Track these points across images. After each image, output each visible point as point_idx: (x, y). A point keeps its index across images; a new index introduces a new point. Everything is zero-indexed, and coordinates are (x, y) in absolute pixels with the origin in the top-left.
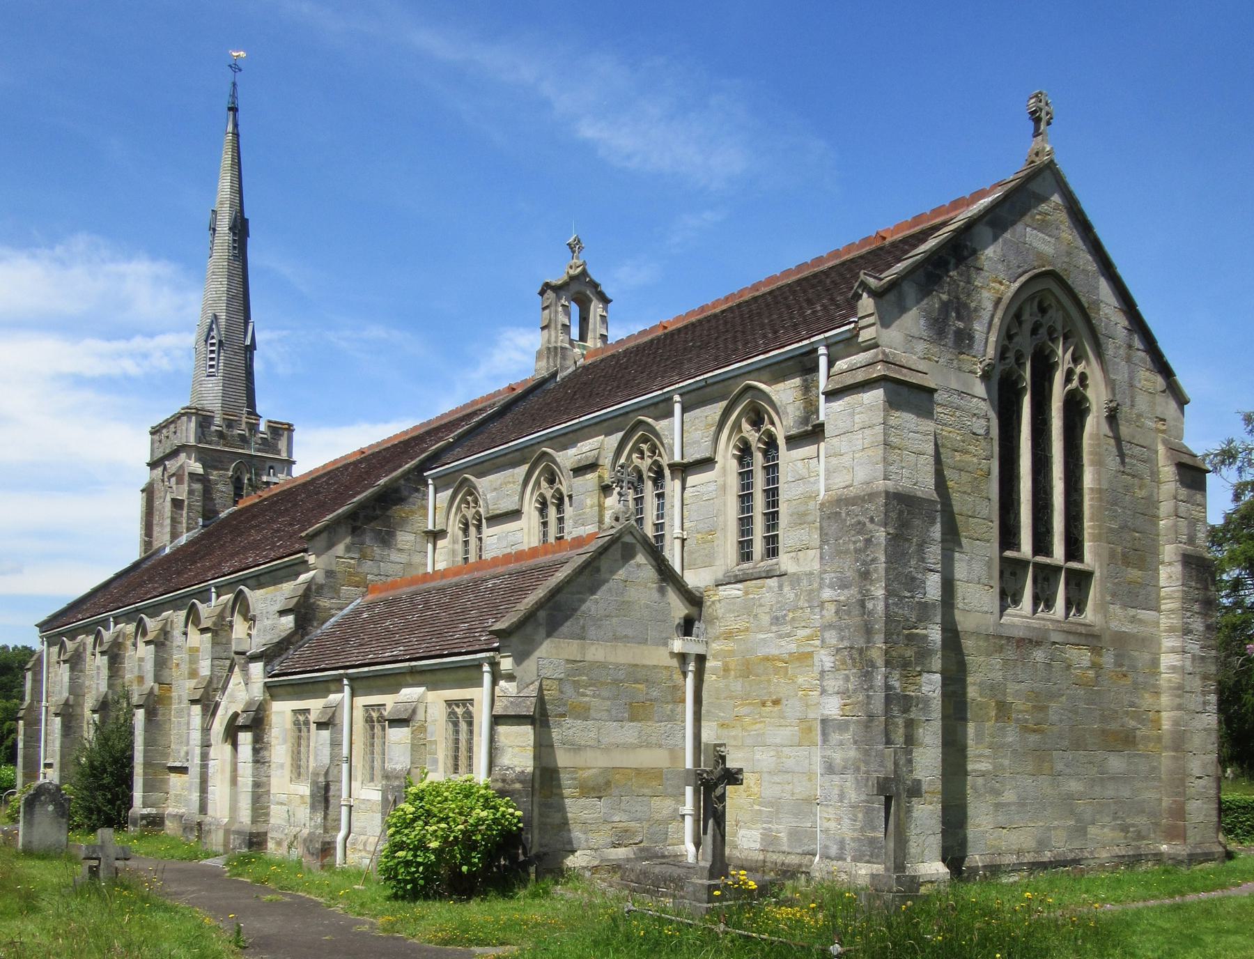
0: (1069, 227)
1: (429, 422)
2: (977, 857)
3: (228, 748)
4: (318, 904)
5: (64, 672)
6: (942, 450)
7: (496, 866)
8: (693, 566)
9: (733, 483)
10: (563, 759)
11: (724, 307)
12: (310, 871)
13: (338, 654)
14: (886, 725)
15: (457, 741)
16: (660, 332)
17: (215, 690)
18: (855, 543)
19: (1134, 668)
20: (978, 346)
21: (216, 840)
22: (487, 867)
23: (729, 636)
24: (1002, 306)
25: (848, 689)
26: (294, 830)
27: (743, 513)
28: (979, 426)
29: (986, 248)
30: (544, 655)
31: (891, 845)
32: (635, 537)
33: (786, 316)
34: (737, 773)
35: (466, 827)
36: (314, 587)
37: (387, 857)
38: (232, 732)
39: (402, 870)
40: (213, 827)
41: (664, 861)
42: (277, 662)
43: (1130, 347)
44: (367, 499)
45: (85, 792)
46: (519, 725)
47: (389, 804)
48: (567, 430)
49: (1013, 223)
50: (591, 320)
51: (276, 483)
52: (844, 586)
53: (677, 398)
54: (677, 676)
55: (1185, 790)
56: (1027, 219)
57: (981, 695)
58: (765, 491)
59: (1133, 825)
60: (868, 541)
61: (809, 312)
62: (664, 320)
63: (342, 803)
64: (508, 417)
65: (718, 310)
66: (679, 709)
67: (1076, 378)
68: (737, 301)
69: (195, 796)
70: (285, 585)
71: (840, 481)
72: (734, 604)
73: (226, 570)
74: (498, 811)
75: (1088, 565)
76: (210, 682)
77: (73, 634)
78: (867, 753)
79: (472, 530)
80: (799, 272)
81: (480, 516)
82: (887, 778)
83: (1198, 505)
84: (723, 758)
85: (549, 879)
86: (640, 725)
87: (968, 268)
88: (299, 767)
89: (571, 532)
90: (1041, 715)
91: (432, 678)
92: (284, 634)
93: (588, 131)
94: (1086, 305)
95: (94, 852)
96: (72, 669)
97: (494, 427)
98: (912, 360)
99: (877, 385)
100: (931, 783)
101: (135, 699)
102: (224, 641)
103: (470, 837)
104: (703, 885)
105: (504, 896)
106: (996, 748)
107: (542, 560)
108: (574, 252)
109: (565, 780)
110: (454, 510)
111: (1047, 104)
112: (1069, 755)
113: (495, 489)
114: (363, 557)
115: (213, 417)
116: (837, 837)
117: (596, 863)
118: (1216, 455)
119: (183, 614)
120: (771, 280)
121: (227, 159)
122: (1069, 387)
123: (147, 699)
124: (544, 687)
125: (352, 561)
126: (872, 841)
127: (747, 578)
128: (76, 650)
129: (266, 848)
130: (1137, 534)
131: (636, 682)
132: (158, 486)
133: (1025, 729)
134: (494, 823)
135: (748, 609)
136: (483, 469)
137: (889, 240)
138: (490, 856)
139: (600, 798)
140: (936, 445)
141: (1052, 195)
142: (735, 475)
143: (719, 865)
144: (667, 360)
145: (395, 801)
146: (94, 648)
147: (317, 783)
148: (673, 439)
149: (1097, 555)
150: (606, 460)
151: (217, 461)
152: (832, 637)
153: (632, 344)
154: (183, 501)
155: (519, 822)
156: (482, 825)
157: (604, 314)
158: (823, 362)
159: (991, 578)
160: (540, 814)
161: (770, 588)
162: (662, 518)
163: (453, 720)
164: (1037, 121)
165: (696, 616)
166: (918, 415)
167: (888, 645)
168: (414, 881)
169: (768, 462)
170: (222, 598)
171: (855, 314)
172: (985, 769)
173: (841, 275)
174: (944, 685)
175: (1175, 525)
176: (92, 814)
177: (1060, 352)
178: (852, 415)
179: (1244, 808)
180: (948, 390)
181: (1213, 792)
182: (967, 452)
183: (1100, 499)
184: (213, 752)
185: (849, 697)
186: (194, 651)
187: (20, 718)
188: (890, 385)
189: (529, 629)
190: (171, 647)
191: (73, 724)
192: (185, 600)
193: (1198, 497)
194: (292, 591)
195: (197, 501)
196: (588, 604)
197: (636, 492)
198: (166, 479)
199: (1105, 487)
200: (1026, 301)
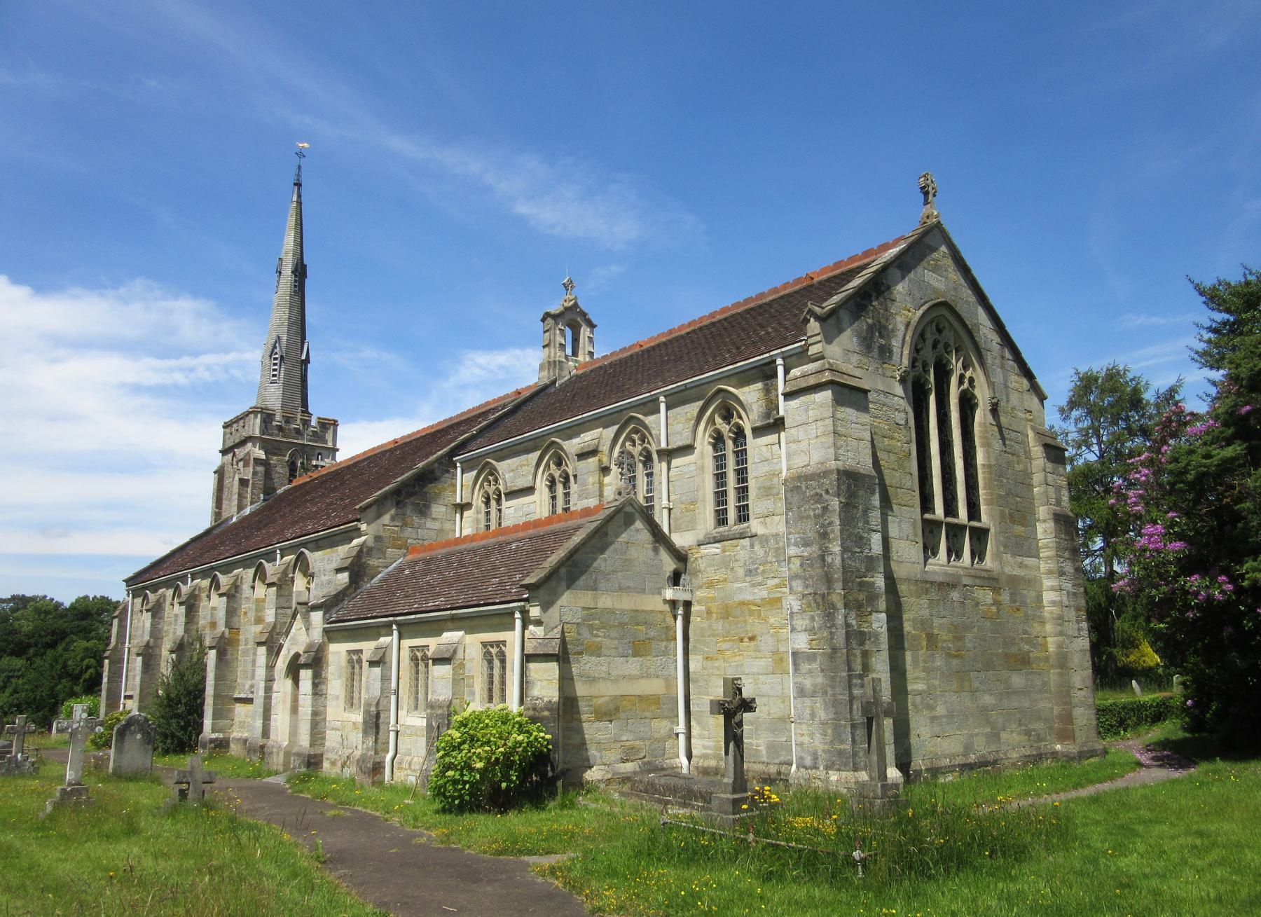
1: (451, 419)
3: (289, 682)
4: (376, 818)
5: (147, 619)
6: (874, 437)
8: (678, 530)
9: (709, 464)
10: (581, 690)
11: (688, 330)
12: (362, 787)
14: (848, 656)
15: (491, 676)
16: (637, 350)
18: (814, 510)
19: (1024, 604)
20: (896, 357)
21: (277, 761)
22: (523, 782)
23: (710, 585)
25: (814, 628)
26: (347, 752)
27: (718, 488)
30: (565, 604)
31: (875, 758)
34: (751, 702)
36: (365, 550)
37: (436, 776)
38: (294, 670)
39: (451, 788)
40: (275, 750)
42: (334, 610)
43: (1003, 357)
44: (409, 479)
45: (161, 720)
46: (546, 662)
47: (434, 731)
49: (915, 267)
50: (581, 341)
51: (322, 467)
52: (806, 544)
53: (662, 399)
54: (670, 619)
55: (1071, 701)
56: (924, 263)
58: (735, 470)
59: (1034, 730)
60: (825, 509)
64: (519, 415)
65: (683, 332)
66: (672, 645)
67: (966, 381)
68: (699, 325)
69: (259, 723)
70: (340, 548)
71: (799, 462)
76: (274, 627)
77: (154, 588)
78: (833, 679)
79: (493, 503)
81: (500, 492)
83: (1061, 476)
84: (740, 690)
85: (572, 794)
86: (641, 659)
87: (885, 299)
89: (577, 504)
90: (960, 644)
92: (340, 588)
93: (523, 209)
94: (970, 327)
95: (185, 776)
96: (153, 617)
97: (508, 422)
101: (207, 642)
102: (286, 594)
103: (509, 758)
104: (728, 799)
105: (537, 808)
107: (556, 526)
108: (567, 290)
109: (583, 706)
110: (478, 487)
111: (932, 182)
112: (982, 675)
113: (513, 471)
114: (405, 525)
115: (275, 415)
116: (811, 749)
117: (609, 776)
119: (251, 571)
121: (291, 221)
123: (219, 641)
124: (565, 630)
125: (396, 529)
126: (840, 753)
127: (723, 538)
128: (158, 601)
130: (1018, 499)
131: (637, 624)
132: (228, 469)
133: (949, 655)
135: (726, 563)
136: (503, 455)
137: (816, 280)
139: (611, 721)
142: (711, 458)
143: (739, 782)
144: (648, 370)
146: (173, 599)
147: (369, 712)
148: (660, 430)
149: (991, 516)
150: (605, 448)
152: (798, 585)
153: (615, 358)
154: (248, 480)
155: (548, 744)
156: (520, 747)
158: (780, 370)
159: (916, 535)
160: (563, 736)
161: (743, 546)
164: (926, 194)
168: (461, 797)
169: (737, 447)
170: (285, 558)
172: (921, 689)
175: (1046, 492)
177: (954, 361)
178: (807, 410)
179: (1103, 710)
180: (877, 391)
183: (990, 473)
184: (276, 686)
185: (815, 634)
188: (836, 387)
189: (553, 583)
190: (241, 598)
191: (152, 662)
192: (254, 560)
195: (259, 480)
196: (598, 561)
198: (235, 463)
199: (993, 463)
200: (928, 323)
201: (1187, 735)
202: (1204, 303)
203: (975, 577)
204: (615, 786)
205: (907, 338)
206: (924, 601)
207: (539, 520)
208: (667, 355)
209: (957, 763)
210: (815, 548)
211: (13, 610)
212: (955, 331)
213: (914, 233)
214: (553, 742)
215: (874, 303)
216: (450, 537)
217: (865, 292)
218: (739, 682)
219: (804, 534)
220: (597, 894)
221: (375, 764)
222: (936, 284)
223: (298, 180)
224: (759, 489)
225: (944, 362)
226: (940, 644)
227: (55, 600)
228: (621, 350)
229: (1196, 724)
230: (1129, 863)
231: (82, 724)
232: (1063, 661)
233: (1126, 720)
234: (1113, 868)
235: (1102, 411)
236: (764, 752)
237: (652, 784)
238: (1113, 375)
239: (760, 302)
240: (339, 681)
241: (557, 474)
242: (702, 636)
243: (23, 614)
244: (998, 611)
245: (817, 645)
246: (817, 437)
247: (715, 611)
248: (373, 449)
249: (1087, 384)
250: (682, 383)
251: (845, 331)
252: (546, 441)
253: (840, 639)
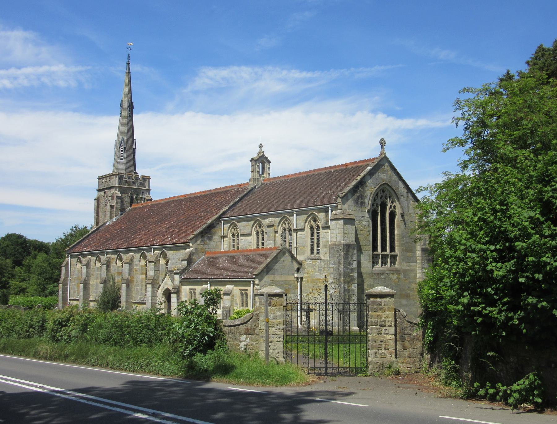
9: (309, 235)
15: (243, 299)
20: (366, 205)
23: (308, 273)
42: (183, 274)
43: (407, 197)
49: (375, 173)
53: (295, 212)
54: (296, 283)
56: (379, 171)
60: (340, 255)
66: (297, 290)
67: (393, 207)
71: (334, 240)
79: (236, 237)
89: (269, 244)
96: (87, 268)
114: (205, 244)
122: (391, 210)
135: (313, 266)
136: (239, 221)
140: (356, 233)
150: (276, 224)
152: (332, 276)
154: (114, 206)
158: (330, 211)
159: (370, 259)
166: (351, 225)
178: (336, 225)
180: (359, 217)
183: (399, 237)
199: (400, 233)
205: (371, 198)
210: (337, 266)
223: (128, 61)
244: (399, 281)
253: (342, 291)
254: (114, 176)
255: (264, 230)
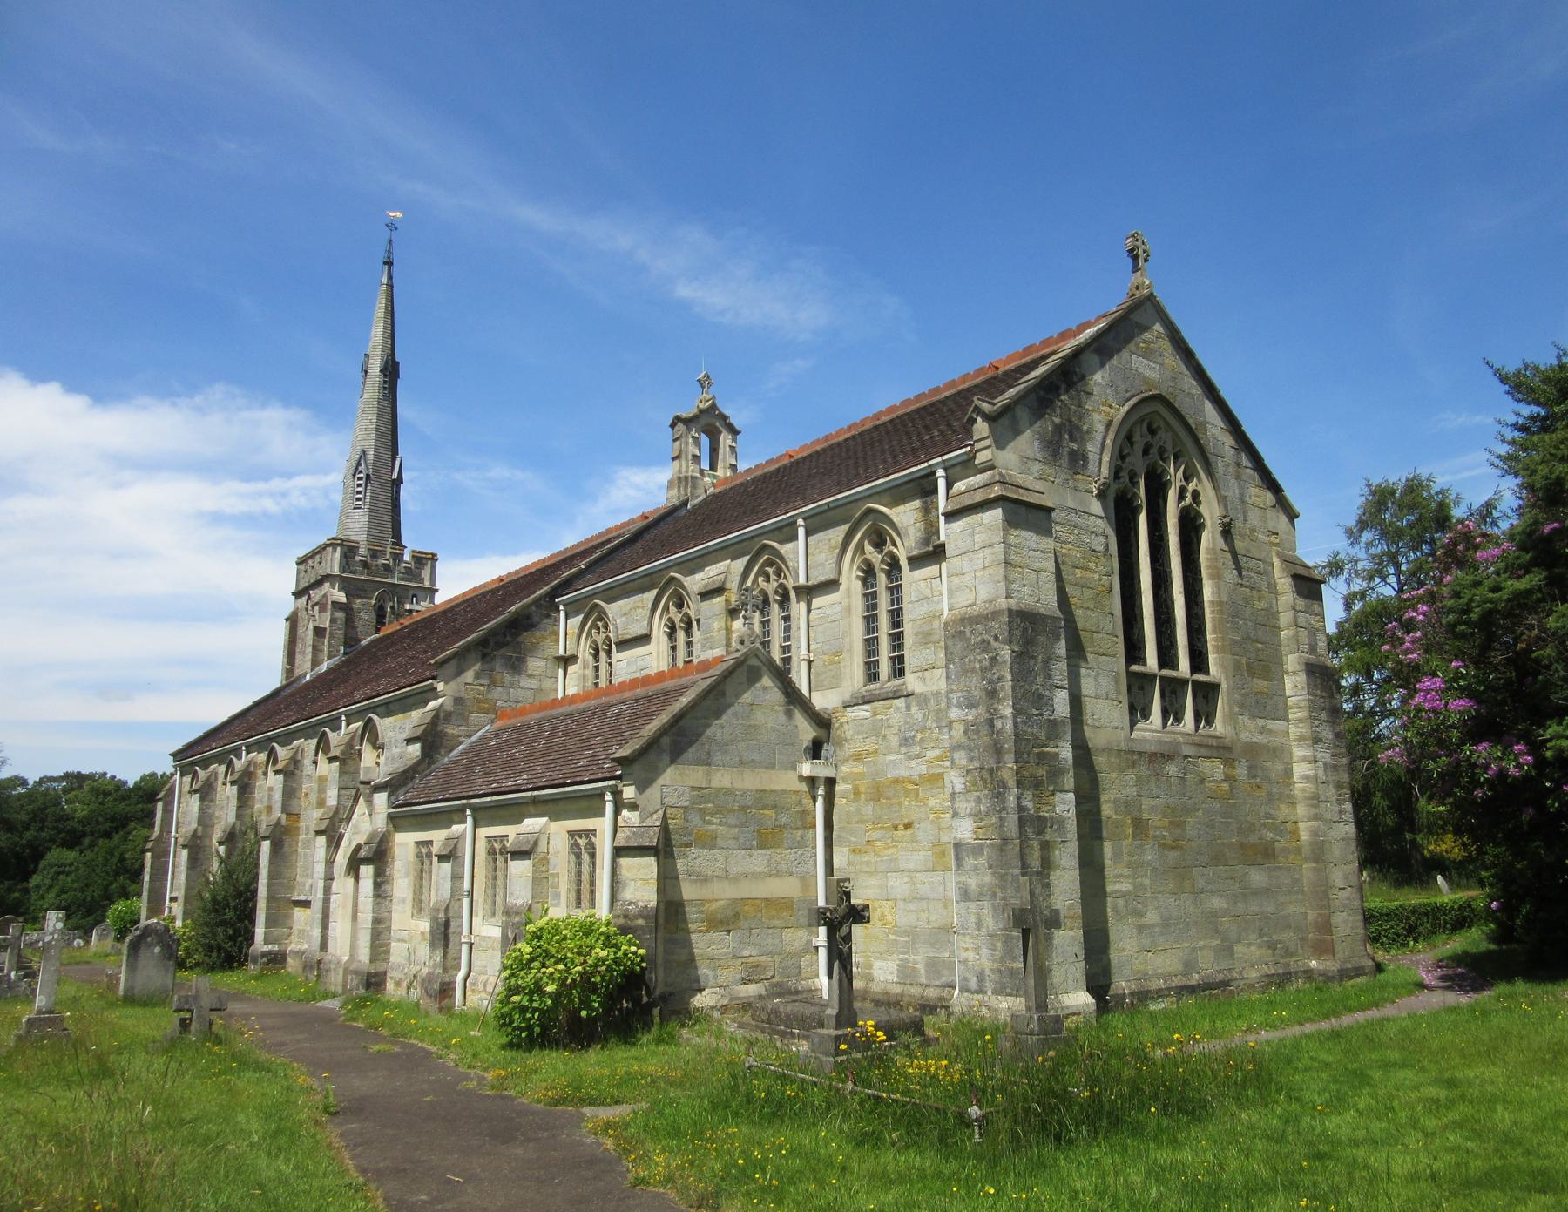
0: (1172, 354)
2: (1123, 984)
3: (351, 881)
5: (194, 803)
6: (1062, 567)
7: (619, 1010)
8: (821, 687)
10: (688, 891)
11: (847, 436)
12: (427, 1014)
13: (462, 783)
15: (579, 874)
16: (786, 461)
17: (341, 820)
18: (980, 661)
19: (1268, 780)
21: (335, 980)
23: (858, 758)
24: (1113, 429)
25: (980, 811)
26: (414, 969)
27: (868, 634)
28: (1098, 543)
29: (1093, 373)
30: (668, 783)
31: (1032, 982)
32: (760, 659)
33: (905, 442)
34: (863, 910)
35: (584, 969)
36: (442, 715)
37: (501, 1002)
38: (354, 866)
40: (332, 966)
41: (795, 998)
42: (401, 791)
43: (1238, 465)
44: (498, 626)
45: (206, 928)
46: (641, 856)
47: (508, 941)
48: (694, 555)
49: (1119, 351)
50: (721, 451)
51: (418, 611)
52: (971, 706)
53: (800, 522)
54: (807, 801)
56: (1132, 346)
57: (1116, 813)
59: (1280, 942)
60: (994, 659)
61: (927, 437)
62: (790, 449)
63: (463, 940)
64: (639, 545)
65: (841, 438)
67: (1189, 495)
68: (860, 430)
69: (317, 932)
70: (414, 712)
71: (963, 600)
72: (862, 725)
73: (357, 697)
74: (620, 950)
75: (1214, 677)
76: (337, 809)
77: (205, 764)
78: (1003, 877)
79: (603, 655)
80: (917, 402)
82: (1023, 909)
83: (1316, 615)
84: (848, 895)
85: (673, 1025)
86: (769, 852)
88: (421, 901)
89: (700, 655)
91: (555, 808)
92: (410, 763)
93: (684, 291)
94: (1194, 427)
95: (187, 1002)
96: (202, 799)
97: (625, 553)
98: (1028, 480)
99: (995, 505)
100: (1070, 907)
101: (263, 830)
102: (352, 769)
103: (590, 979)
104: (829, 1036)
105: (626, 1042)
106: (1135, 867)
107: (668, 684)
108: (703, 387)
109: (691, 912)
110: (584, 635)
111: (1143, 243)
112: (1210, 871)
113: (625, 614)
114: (493, 683)
117: (725, 1002)
118: (1324, 567)
120: (891, 409)
121: (380, 308)
124: (668, 816)
125: (482, 688)
126: (1012, 972)
128: (208, 779)
129: (385, 989)
130: (1260, 645)
131: (764, 808)
132: (303, 615)
133: (1164, 846)
134: (616, 962)
135: (877, 730)
136: (613, 595)
137: (1002, 370)
138: (611, 1000)
139: (729, 931)
140: (1056, 562)
141: (1154, 324)
142: (860, 596)
143: (846, 1012)
145: (515, 939)
148: (798, 562)
149: (1222, 666)
150: (733, 585)
151: (360, 590)
152: (961, 757)
153: (760, 473)
154: (325, 629)
155: (642, 961)
156: (602, 965)
157: (734, 444)
158: (942, 484)
159: (1118, 693)
160: (665, 951)
162: (789, 640)
163: (575, 850)
164: (1135, 258)
165: (824, 739)
166: (1038, 533)
167: (1019, 765)
168: (529, 1028)
170: (351, 726)
171: (971, 438)
172: (1125, 889)
173: (957, 403)
174: (1078, 804)
175: (1296, 637)
176: (212, 952)
177: (1172, 470)
178: (972, 534)
179: (1387, 915)
180: (1066, 509)
181: (1357, 903)
182: (1087, 569)
183: (1221, 612)
184: (335, 887)
185: (982, 820)
186: (322, 779)
187: (148, 850)
189: (652, 756)
192: (317, 728)
193: (1316, 607)
194: (421, 718)
195: (339, 629)
197: (762, 614)
199: (1225, 599)
201: (1492, 947)
202: (1508, 393)
203: (1199, 745)
204: (733, 1014)
205: (1109, 442)
206: (1130, 777)
207: (649, 677)
208: (816, 467)
209: (1173, 985)
210: (981, 710)
211: (66, 791)
212: (1173, 430)
213: (1121, 307)
214: (650, 958)
215: (1062, 398)
216: (552, 696)
217: (1051, 383)
218: (846, 884)
219: (969, 692)
220: (645, 1159)
221: (443, 984)
222: (1148, 373)
223: (389, 257)
224: (916, 635)
225: (1159, 472)
226: (1151, 833)
227: (118, 778)
228: (767, 462)
229: (1503, 934)
230: (1341, 1124)
231: (56, 936)
232: (1319, 853)
233: (1416, 927)
234: (1318, 1130)
235: (1399, 533)
236: (923, 970)
237: (776, 1012)
238: (1414, 487)
239: (934, 399)
240: (406, 880)
241: (677, 618)
242: (848, 823)
243: (76, 796)
245: (984, 834)
246: (985, 568)
247: (863, 790)
248: (475, 589)
249: (1381, 498)
250: (824, 502)
251: (1023, 432)
252: (663, 576)
254: (330, 549)
255: (692, 613)
